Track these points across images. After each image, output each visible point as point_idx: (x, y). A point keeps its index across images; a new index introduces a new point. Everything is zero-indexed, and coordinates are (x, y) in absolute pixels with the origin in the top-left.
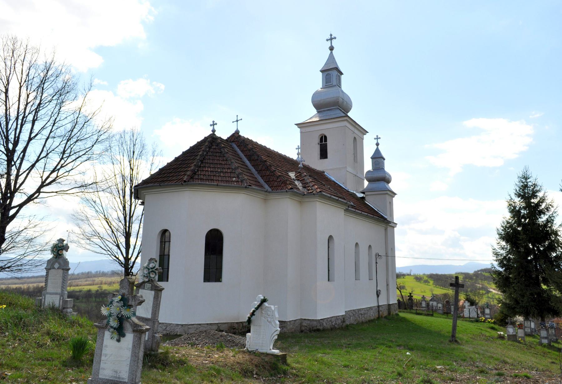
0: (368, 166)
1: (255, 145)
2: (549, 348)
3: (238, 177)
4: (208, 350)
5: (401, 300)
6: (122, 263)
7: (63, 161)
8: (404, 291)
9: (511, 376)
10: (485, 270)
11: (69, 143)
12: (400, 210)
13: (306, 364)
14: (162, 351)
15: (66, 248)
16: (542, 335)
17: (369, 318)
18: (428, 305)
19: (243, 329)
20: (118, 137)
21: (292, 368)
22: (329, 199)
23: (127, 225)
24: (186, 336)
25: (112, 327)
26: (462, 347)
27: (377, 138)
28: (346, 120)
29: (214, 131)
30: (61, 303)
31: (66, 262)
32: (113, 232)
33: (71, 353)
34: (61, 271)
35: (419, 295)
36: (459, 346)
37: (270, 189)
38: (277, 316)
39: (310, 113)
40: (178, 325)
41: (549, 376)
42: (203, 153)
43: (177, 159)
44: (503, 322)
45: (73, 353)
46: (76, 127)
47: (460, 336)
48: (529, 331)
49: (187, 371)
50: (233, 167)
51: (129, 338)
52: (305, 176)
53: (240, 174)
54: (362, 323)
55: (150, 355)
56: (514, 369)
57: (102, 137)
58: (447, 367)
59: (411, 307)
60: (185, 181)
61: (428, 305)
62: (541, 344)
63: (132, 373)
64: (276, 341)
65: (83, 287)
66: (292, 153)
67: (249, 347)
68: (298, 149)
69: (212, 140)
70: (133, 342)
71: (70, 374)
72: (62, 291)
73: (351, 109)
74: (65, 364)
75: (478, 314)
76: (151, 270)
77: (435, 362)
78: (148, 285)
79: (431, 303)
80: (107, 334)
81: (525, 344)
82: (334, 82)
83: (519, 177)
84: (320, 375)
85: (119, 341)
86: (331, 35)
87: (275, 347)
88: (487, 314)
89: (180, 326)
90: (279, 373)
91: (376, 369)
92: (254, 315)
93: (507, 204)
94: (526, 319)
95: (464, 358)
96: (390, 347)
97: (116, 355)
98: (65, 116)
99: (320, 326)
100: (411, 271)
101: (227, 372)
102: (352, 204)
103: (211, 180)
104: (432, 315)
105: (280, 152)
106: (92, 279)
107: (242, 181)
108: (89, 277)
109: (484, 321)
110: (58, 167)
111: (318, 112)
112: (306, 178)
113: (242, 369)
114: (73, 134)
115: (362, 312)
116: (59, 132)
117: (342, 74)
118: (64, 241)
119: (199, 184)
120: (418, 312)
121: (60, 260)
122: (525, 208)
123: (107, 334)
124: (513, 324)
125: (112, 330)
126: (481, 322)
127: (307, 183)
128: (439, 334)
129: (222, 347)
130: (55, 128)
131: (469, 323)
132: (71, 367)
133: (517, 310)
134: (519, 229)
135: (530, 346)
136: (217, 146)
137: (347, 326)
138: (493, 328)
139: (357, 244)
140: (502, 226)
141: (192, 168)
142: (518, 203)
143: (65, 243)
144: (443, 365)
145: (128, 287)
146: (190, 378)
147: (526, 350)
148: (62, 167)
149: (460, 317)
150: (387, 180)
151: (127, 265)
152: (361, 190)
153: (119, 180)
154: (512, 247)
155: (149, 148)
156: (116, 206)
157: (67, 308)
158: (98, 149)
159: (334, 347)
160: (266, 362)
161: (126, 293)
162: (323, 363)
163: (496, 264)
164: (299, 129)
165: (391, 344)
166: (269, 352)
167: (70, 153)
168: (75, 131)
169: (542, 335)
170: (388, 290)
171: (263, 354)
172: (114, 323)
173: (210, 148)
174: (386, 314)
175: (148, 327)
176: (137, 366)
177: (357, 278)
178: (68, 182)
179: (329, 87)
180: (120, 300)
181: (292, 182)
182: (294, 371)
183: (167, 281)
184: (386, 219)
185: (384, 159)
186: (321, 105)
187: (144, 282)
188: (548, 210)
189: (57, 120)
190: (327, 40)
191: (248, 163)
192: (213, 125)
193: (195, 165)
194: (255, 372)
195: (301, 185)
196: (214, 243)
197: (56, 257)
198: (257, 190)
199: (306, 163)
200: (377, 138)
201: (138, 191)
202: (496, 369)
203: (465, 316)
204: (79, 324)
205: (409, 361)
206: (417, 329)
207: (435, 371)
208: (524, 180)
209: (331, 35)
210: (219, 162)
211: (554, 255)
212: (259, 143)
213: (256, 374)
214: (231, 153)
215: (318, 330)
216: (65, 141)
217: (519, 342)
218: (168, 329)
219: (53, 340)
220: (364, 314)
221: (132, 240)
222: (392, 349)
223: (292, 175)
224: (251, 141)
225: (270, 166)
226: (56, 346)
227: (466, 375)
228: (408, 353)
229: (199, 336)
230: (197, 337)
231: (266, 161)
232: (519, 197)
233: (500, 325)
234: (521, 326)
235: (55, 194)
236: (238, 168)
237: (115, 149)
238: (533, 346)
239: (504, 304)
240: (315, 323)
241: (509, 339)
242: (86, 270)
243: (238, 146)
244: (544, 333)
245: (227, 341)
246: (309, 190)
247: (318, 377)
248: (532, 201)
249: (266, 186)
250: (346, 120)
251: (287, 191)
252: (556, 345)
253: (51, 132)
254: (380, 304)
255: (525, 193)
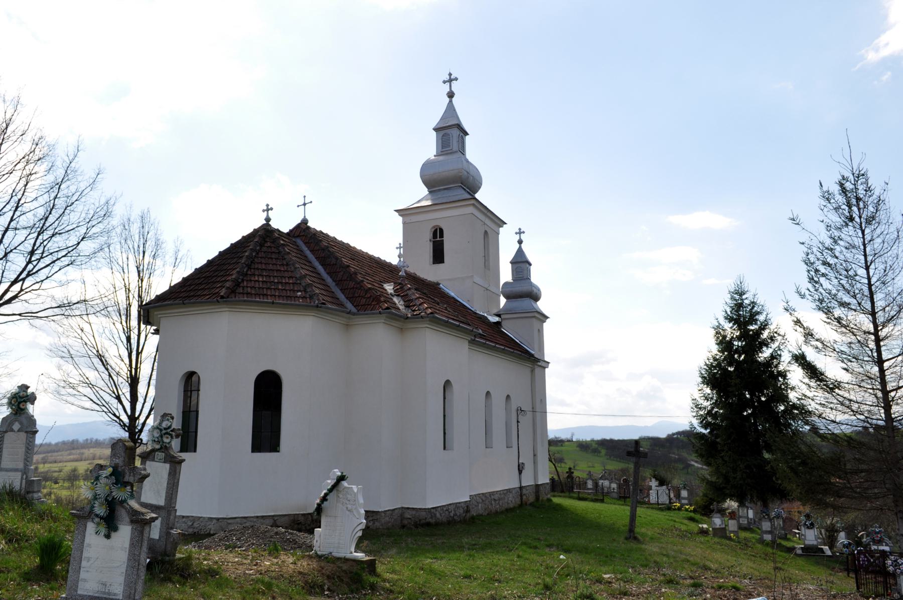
0: (506, 275)
1: (332, 241)
2: (773, 548)
3: (305, 291)
4: (254, 554)
5: (556, 477)
6: (125, 425)
7: (30, 267)
8: (563, 465)
9: (712, 588)
10: (683, 433)
11: (40, 237)
12: (555, 343)
13: (406, 574)
14: (182, 556)
15: (32, 399)
16: (764, 528)
17: (506, 506)
18: (596, 485)
19: (308, 523)
20: (119, 230)
21: (384, 580)
22: (446, 324)
23: (134, 366)
24: (222, 534)
25: (97, 516)
26: (643, 546)
27: (520, 232)
28: (473, 205)
29: (268, 220)
30: (23, 486)
31: (32, 421)
32: (110, 376)
33: (38, 560)
34: (23, 435)
35: (583, 471)
36: (640, 546)
37: (354, 310)
38: (361, 501)
39: (417, 193)
40: (211, 519)
41: (768, 587)
42: (251, 254)
43: (210, 263)
44: (706, 510)
45: (41, 560)
46: (53, 212)
47: (643, 530)
48: (746, 522)
49: (219, 586)
50: (298, 276)
51: (125, 532)
52: (410, 289)
53: (309, 285)
54: (497, 513)
55: (163, 562)
56: (717, 578)
57: (94, 230)
58: (619, 576)
59: (571, 490)
60: (222, 297)
61: (596, 485)
62: (762, 541)
63: (129, 585)
64: (361, 540)
65: (65, 464)
66: (391, 257)
67: (317, 549)
68: (400, 248)
69: (264, 236)
70: (131, 539)
71: (35, 591)
72: (26, 465)
73: (479, 188)
74: (29, 577)
75: (670, 499)
76: (164, 432)
77: (602, 568)
78: (160, 455)
79: (601, 482)
80: (91, 527)
81: (739, 542)
82: (455, 146)
83: (730, 292)
84: (426, 590)
85: (108, 536)
86: (450, 74)
87: (358, 548)
88: (684, 498)
89: (215, 521)
90: (364, 588)
91: (512, 579)
92: (326, 500)
93: (713, 332)
94: (742, 504)
95: (645, 563)
96: (536, 547)
97: (104, 558)
98: (34, 195)
99: (432, 518)
100: (573, 435)
101: (283, 587)
102: (480, 331)
103: (263, 295)
104: (602, 501)
105: (371, 253)
106: (78, 451)
107: (311, 297)
108: (73, 449)
109: (679, 509)
110: (23, 276)
111: (430, 192)
112: (410, 292)
113: (306, 583)
114: (47, 224)
115: (496, 497)
116: (23, 221)
117: (466, 134)
118: (28, 387)
119: (245, 301)
120: (581, 495)
121: (23, 418)
122: (739, 338)
123: (91, 527)
124: (722, 512)
125: (97, 520)
126: (675, 509)
127: (412, 300)
128: (610, 529)
129: (277, 550)
130: (18, 213)
131: (658, 512)
132: (37, 582)
133: (728, 492)
134: (731, 369)
135: (745, 545)
136: (273, 242)
137: (473, 518)
138: (692, 519)
139: (488, 393)
140: (706, 365)
141: (234, 277)
142: (729, 330)
143: (30, 391)
144: (614, 573)
145: (123, 454)
146: (224, 595)
147: (739, 551)
148: (28, 275)
149: (644, 503)
150: (534, 296)
151: (132, 427)
152: (495, 311)
153: (121, 297)
154: (719, 397)
155: (169, 248)
156: (116, 336)
157: (34, 492)
158: (87, 247)
159: (452, 549)
160: (345, 571)
161: (121, 464)
162: (432, 572)
163: (696, 422)
164: (401, 219)
165: (538, 544)
166: (348, 556)
167: (43, 253)
168: (51, 219)
169: (764, 528)
170: (535, 462)
171: (339, 559)
172: (100, 510)
173: (261, 246)
174: (532, 499)
175: (154, 515)
176: (138, 575)
177: (488, 446)
178: (39, 301)
179: (447, 154)
180: (111, 475)
181: (388, 299)
182: (388, 585)
183: (195, 451)
184: (532, 355)
185: (530, 265)
186: (434, 180)
187: (153, 451)
188: (772, 340)
189: (21, 202)
190: (444, 82)
191: (320, 268)
192: (268, 210)
193: (238, 272)
194: (326, 587)
195: (402, 302)
196: (268, 389)
197: (16, 414)
198: (336, 310)
199: (411, 270)
200: (520, 232)
201: (150, 312)
202: (691, 578)
203: (652, 502)
204: (52, 517)
205: (562, 568)
206: (579, 523)
207: (599, 581)
208: (737, 297)
209: (450, 74)
210: (278, 268)
211: (782, 408)
212: (339, 238)
213: (329, 590)
214: (294, 254)
215: (428, 524)
216: (36, 234)
217: (730, 539)
218: (196, 525)
219: (10, 541)
220: (499, 499)
221: (141, 389)
222: (538, 550)
223: (389, 288)
224: (327, 235)
225: (356, 274)
226: (15, 549)
227: (647, 587)
228: (562, 557)
229: (243, 535)
230: (240, 536)
231: (348, 266)
232: (730, 322)
233: (703, 515)
234: (733, 515)
235: (18, 317)
236: (305, 276)
237: (117, 252)
238: (750, 544)
239: (709, 483)
240: (424, 513)
241: (715, 535)
242: (70, 438)
243: (305, 243)
244: (766, 525)
245: (285, 542)
246: (414, 311)
247: (423, 593)
248: (751, 328)
249: (349, 306)
250: (473, 205)
251: (380, 313)
252: (784, 543)
253: (12, 220)
254: (523, 485)
255: (739, 315)
